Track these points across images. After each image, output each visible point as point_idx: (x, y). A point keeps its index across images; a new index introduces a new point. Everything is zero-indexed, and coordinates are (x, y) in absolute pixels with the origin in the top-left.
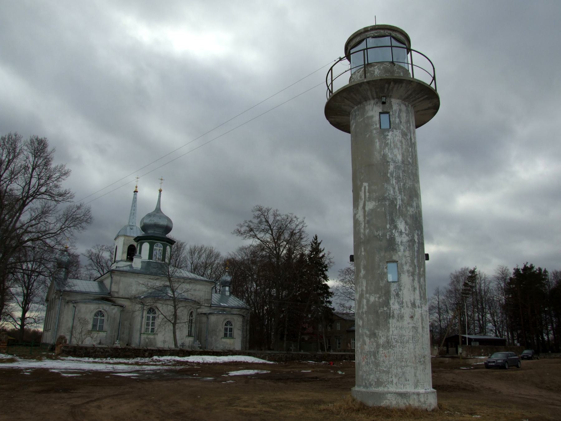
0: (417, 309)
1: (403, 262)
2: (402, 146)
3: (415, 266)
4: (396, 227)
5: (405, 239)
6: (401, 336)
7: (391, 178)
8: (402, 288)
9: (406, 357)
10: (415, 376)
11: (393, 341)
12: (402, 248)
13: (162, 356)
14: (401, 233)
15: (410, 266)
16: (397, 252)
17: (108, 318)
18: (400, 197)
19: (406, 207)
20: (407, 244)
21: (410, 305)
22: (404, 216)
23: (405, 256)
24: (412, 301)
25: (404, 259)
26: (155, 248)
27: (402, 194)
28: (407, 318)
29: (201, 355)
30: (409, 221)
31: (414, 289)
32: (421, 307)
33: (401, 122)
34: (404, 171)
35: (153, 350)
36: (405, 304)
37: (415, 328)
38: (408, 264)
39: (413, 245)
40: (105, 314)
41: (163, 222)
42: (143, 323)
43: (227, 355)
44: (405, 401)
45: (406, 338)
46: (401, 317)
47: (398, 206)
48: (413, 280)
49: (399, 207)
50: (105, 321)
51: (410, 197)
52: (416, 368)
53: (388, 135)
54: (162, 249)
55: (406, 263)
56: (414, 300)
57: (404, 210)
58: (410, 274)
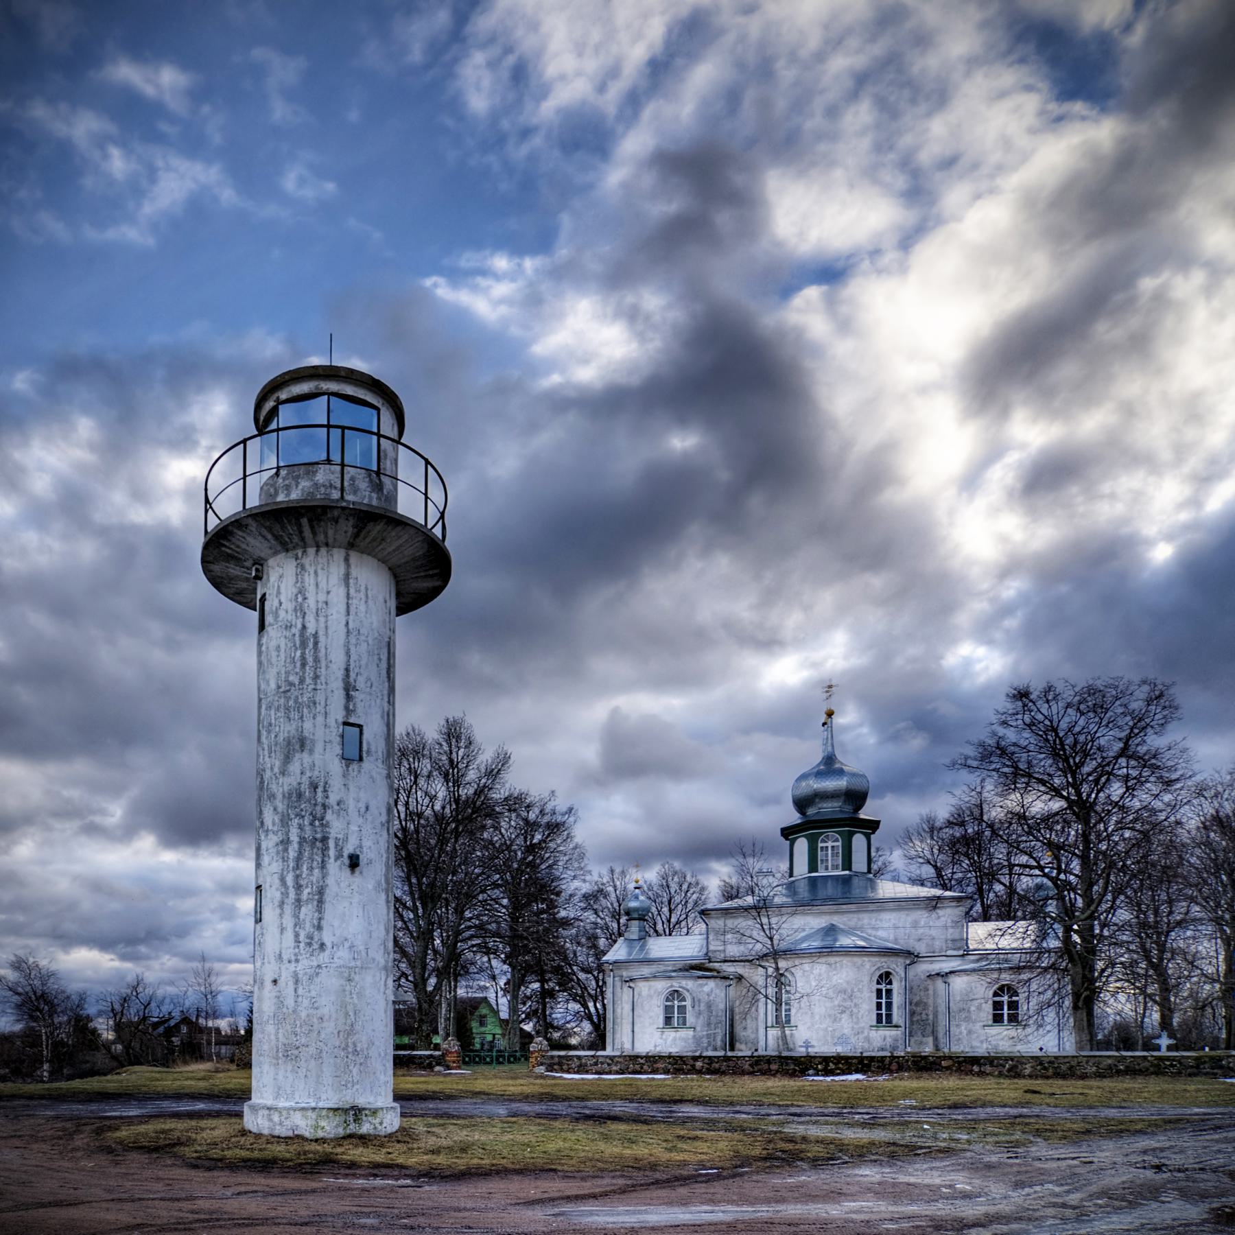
0: (288, 965)
26: (820, 845)
34: (278, 709)
39: (286, 850)
40: (686, 994)
41: (839, 783)
54: (839, 844)
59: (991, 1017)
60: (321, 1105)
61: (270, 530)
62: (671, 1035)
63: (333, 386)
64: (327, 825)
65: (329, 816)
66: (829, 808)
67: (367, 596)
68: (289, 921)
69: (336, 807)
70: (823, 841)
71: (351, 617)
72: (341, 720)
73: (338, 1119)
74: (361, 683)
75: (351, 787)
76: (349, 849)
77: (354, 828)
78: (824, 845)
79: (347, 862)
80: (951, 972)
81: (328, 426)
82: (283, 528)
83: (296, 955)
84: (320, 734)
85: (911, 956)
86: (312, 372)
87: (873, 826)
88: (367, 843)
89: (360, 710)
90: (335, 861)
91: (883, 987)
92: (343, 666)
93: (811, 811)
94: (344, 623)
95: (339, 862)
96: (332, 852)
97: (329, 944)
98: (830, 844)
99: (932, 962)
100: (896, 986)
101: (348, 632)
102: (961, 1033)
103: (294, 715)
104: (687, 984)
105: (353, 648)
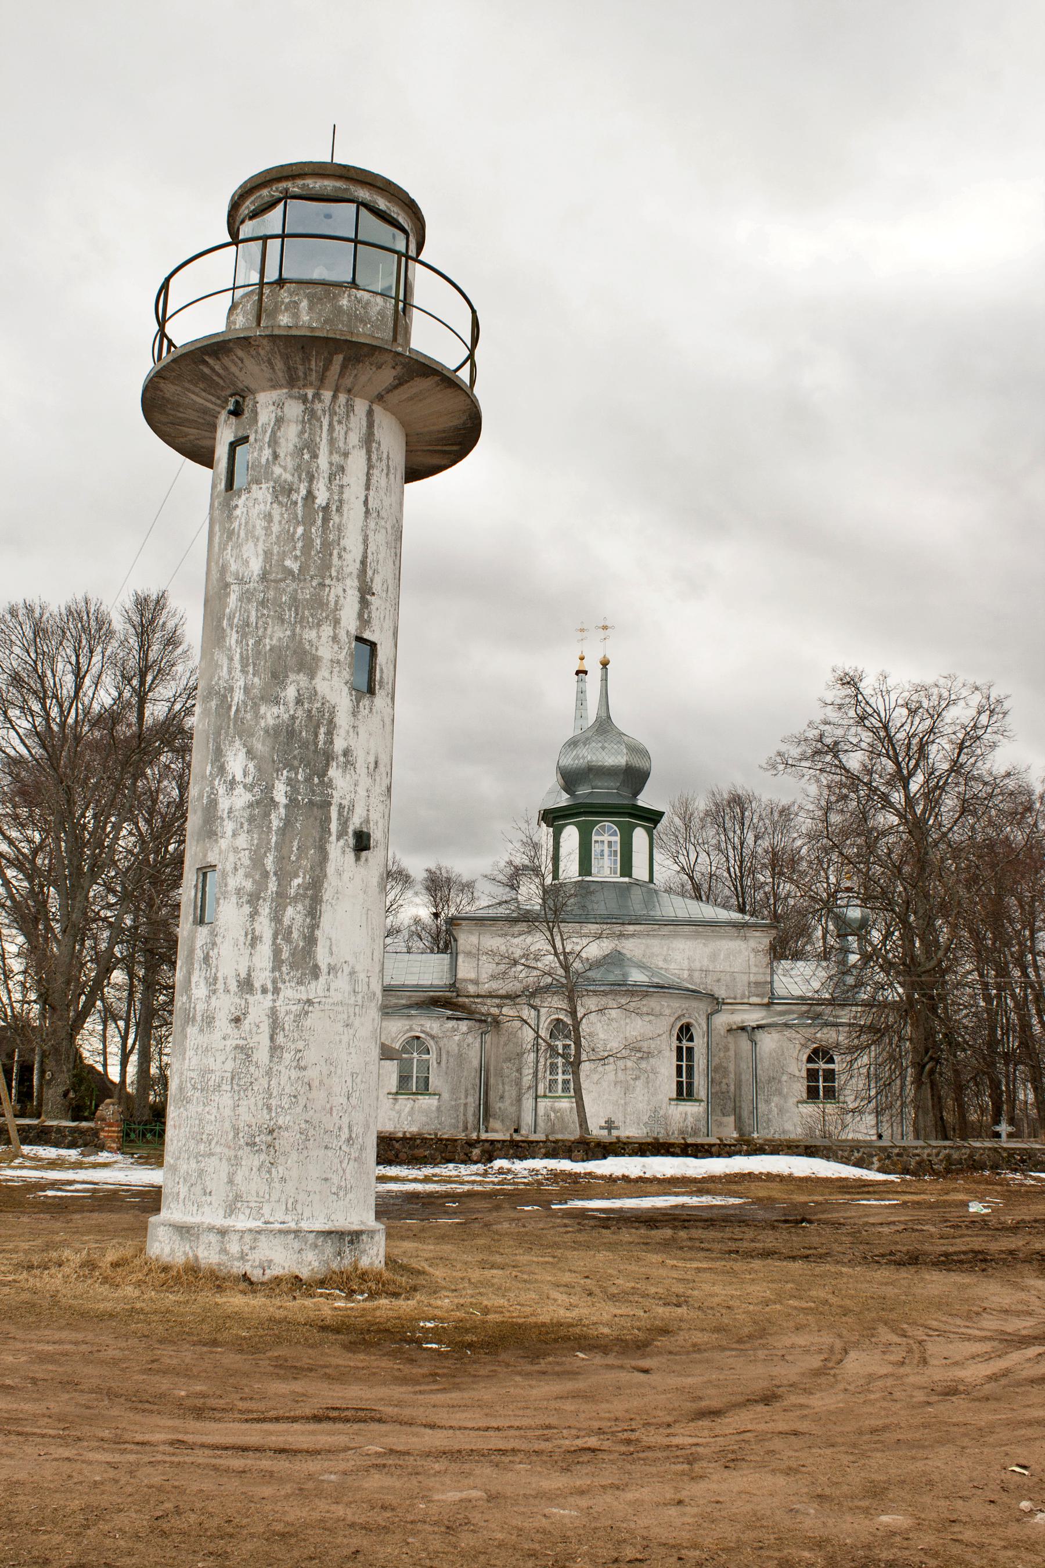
0: (259, 996)
1: (229, 867)
2: (268, 529)
3: (266, 875)
4: (222, 770)
5: (241, 798)
6: (205, 1072)
7: (228, 630)
8: (219, 940)
9: (209, 1129)
10: (231, 1182)
11: (189, 1085)
12: (229, 826)
13: (522, 1158)
14: (232, 784)
15: (247, 876)
16: (216, 841)
17: (439, 1055)
18: (241, 683)
19: (256, 707)
20: (246, 814)
21: (233, 986)
22: (244, 732)
23: (236, 850)
24: (243, 975)
25: (232, 858)
26: (594, 838)
27: (247, 673)
28: (222, 1024)
29: (643, 1155)
30: (259, 746)
31: (254, 940)
32: (276, 991)
33: (276, 456)
34: (263, 603)
35: (492, 1142)
36: (220, 985)
37: (245, 1051)
38: (241, 872)
39: (267, 814)
40: (431, 1044)
41: (614, 758)
42: (541, 1067)
43: (730, 1155)
44: (187, 1248)
45: (214, 1079)
46: (209, 1020)
47: (234, 709)
48: (253, 915)
49: (237, 710)
50: (433, 1064)
51: (274, 675)
52: (235, 1162)
53: (237, 506)
54: (617, 839)
55: (236, 869)
56: (250, 971)
57: (249, 716)
58: (245, 899)
59: (804, 1089)
60: (305, 1225)
61: (286, 358)
62: (405, 1103)
63: (363, 194)
64: (330, 785)
65: (333, 772)
66: (604, 792)
67: (388, 466)
68: (264, 927)
69: (342, 759)
70: (598, 834)
71: (371, 493)
72: (353, 632)
73: (329, 1249)
74: (377, 587)
75: (361, 730)
76: (355, 822)
77: (362, 792)
78: (599, 838)
79: (351, 841)
80: (759, 1027)
81: (356, 241)
82: (306, 359)
83: (274, 982)
84: (326, 652)
85: (717, 1003)
86: (344, 172)
87: (652, 818)
88: (373, 816)
89: (375, 623)
90: (338, 840)
91: (685, 1044)
92: (359, 558)
93: (582, 791)
94: (363, 498)
95: (342, 842)
96: (334, 826)
97: (324, 968)
98: (606, 838)
99: (733, 1012)
100: (699, 1044)
101: (367, 512)
102: (770, 1111)
103: (289, 615)
104: (431, 1025)
105: (371, 534)
